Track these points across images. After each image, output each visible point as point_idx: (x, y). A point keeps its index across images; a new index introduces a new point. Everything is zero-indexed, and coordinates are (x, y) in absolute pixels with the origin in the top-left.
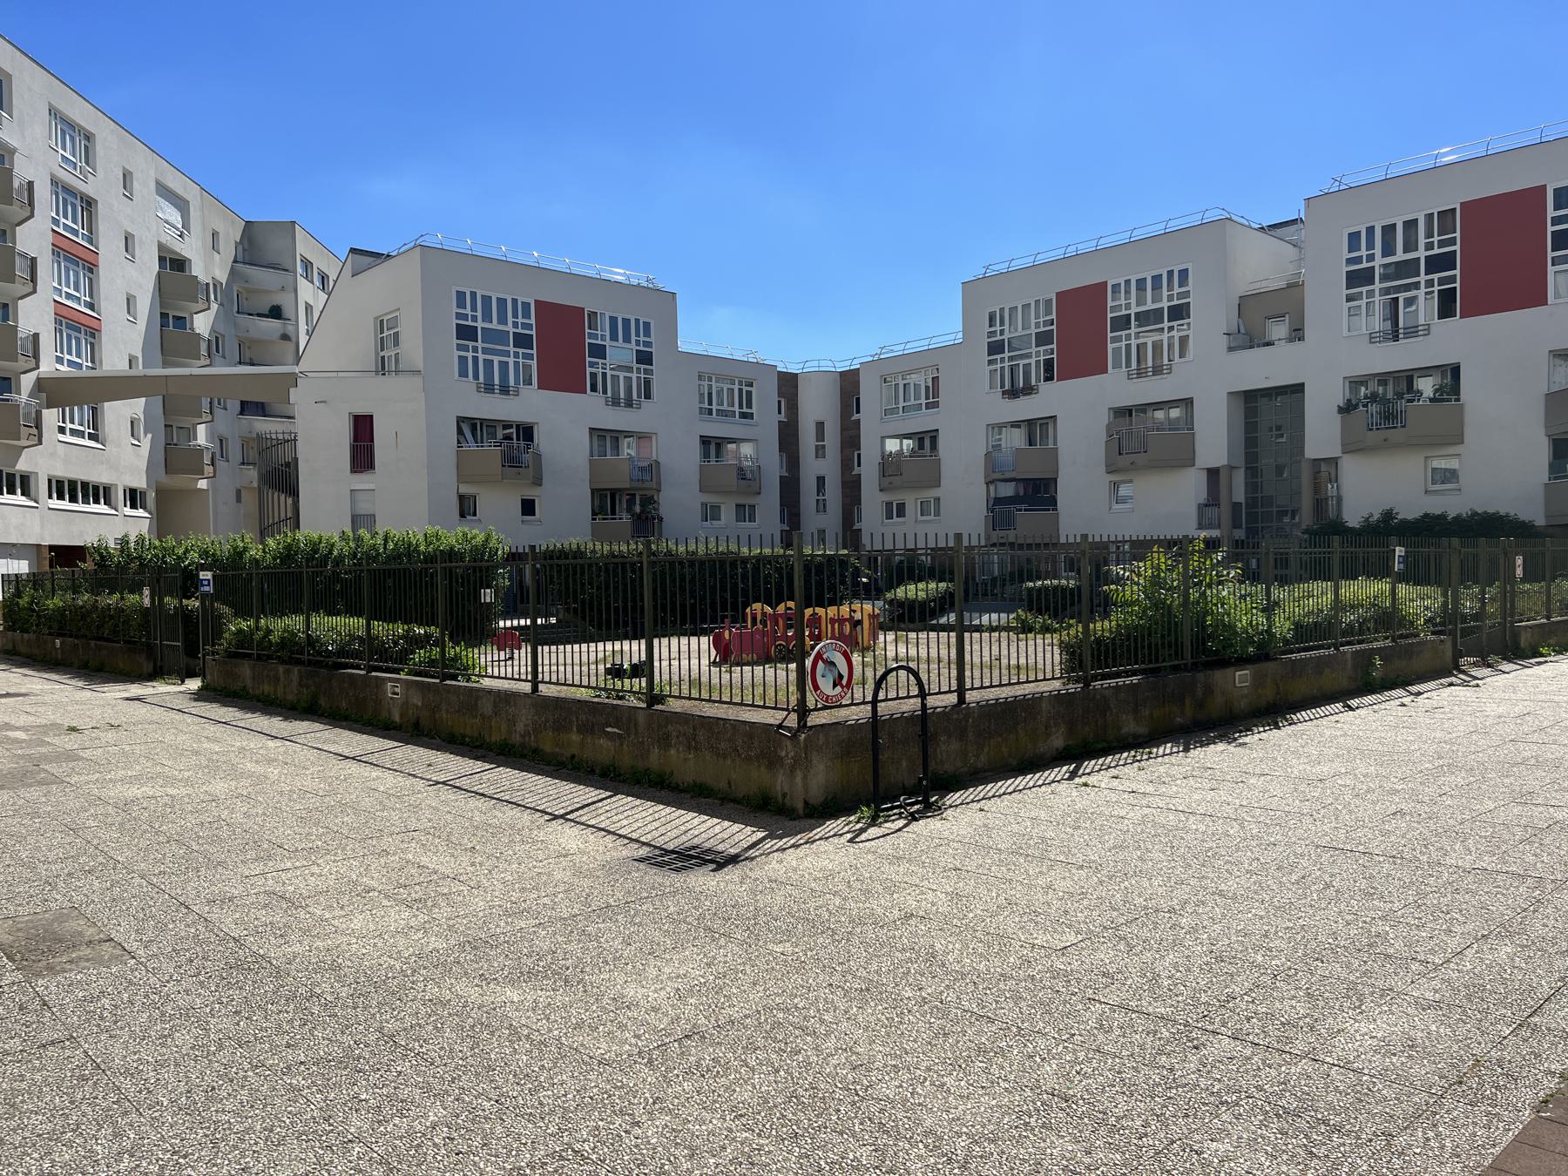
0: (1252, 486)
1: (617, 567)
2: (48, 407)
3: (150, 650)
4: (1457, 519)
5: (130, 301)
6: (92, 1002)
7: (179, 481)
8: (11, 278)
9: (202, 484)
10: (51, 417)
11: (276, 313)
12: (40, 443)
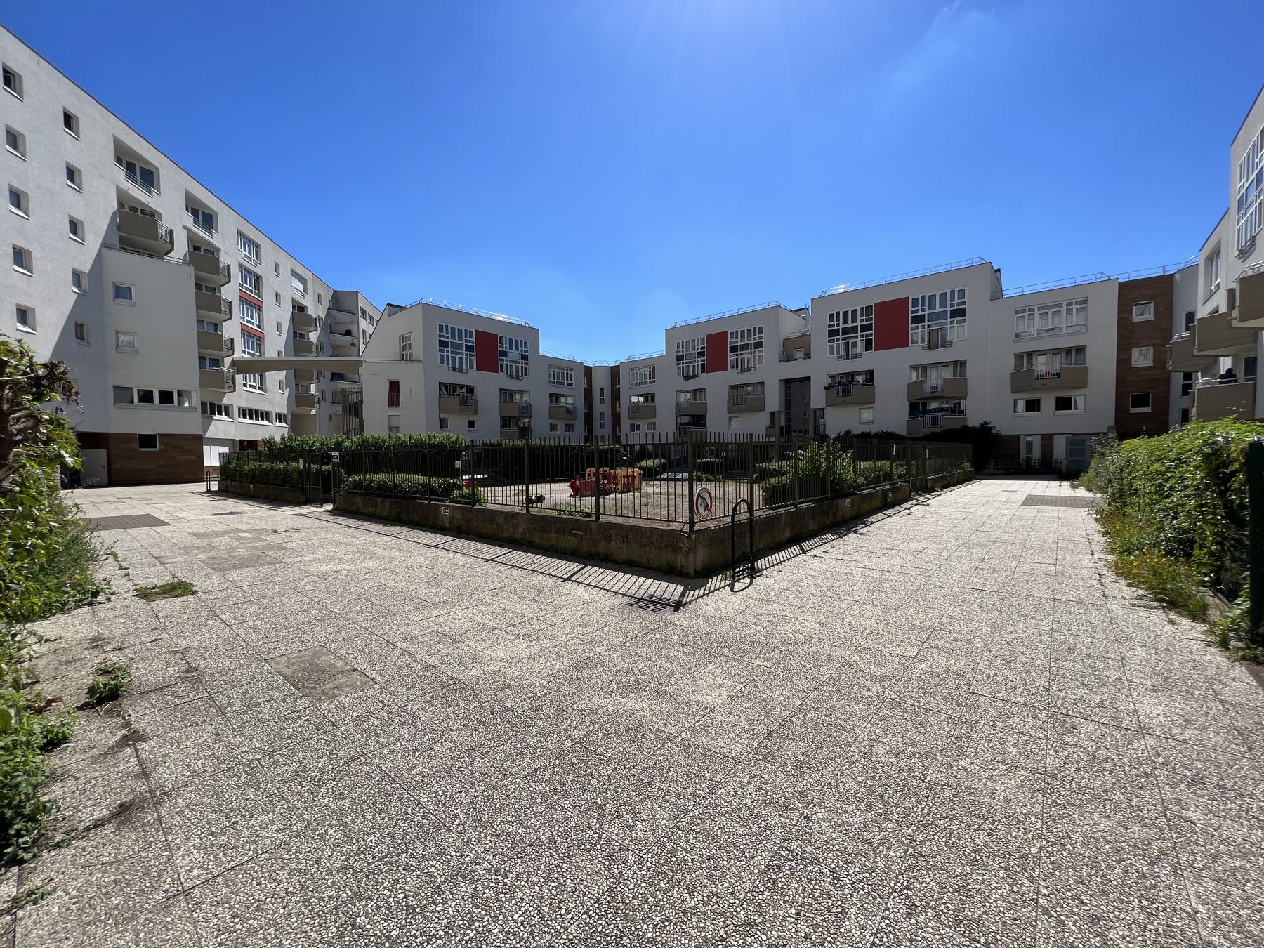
0: (788, 420)
1: (516, 450)
3: (303, 491)
4: (876, 434)
5: (278, 325)
6: (364, 721)
7: (303, 410)
8: (219, 311)
9: (313, 412)
10: (239, 378)
11: (348, 333)
12: (235, 391)
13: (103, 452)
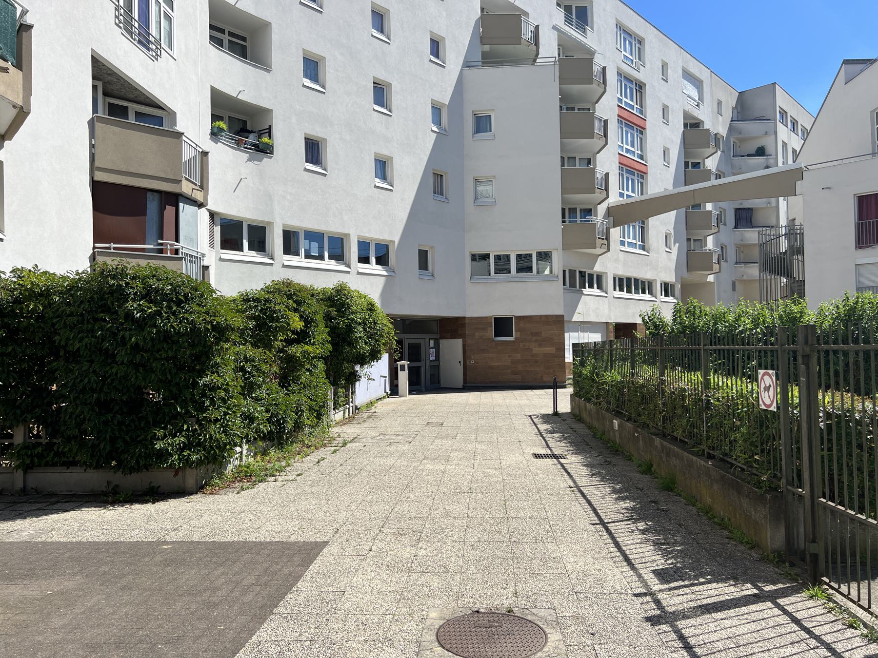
2: (614, 227)
5: (666, 152)
8: (591, 135)
10: (615, 233)
11: (761, 152)
13: (459, 342)
